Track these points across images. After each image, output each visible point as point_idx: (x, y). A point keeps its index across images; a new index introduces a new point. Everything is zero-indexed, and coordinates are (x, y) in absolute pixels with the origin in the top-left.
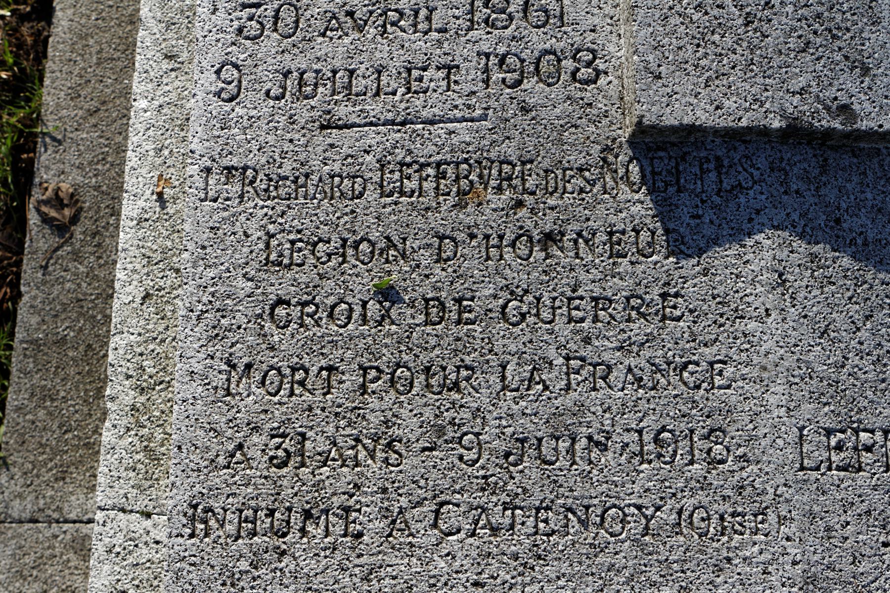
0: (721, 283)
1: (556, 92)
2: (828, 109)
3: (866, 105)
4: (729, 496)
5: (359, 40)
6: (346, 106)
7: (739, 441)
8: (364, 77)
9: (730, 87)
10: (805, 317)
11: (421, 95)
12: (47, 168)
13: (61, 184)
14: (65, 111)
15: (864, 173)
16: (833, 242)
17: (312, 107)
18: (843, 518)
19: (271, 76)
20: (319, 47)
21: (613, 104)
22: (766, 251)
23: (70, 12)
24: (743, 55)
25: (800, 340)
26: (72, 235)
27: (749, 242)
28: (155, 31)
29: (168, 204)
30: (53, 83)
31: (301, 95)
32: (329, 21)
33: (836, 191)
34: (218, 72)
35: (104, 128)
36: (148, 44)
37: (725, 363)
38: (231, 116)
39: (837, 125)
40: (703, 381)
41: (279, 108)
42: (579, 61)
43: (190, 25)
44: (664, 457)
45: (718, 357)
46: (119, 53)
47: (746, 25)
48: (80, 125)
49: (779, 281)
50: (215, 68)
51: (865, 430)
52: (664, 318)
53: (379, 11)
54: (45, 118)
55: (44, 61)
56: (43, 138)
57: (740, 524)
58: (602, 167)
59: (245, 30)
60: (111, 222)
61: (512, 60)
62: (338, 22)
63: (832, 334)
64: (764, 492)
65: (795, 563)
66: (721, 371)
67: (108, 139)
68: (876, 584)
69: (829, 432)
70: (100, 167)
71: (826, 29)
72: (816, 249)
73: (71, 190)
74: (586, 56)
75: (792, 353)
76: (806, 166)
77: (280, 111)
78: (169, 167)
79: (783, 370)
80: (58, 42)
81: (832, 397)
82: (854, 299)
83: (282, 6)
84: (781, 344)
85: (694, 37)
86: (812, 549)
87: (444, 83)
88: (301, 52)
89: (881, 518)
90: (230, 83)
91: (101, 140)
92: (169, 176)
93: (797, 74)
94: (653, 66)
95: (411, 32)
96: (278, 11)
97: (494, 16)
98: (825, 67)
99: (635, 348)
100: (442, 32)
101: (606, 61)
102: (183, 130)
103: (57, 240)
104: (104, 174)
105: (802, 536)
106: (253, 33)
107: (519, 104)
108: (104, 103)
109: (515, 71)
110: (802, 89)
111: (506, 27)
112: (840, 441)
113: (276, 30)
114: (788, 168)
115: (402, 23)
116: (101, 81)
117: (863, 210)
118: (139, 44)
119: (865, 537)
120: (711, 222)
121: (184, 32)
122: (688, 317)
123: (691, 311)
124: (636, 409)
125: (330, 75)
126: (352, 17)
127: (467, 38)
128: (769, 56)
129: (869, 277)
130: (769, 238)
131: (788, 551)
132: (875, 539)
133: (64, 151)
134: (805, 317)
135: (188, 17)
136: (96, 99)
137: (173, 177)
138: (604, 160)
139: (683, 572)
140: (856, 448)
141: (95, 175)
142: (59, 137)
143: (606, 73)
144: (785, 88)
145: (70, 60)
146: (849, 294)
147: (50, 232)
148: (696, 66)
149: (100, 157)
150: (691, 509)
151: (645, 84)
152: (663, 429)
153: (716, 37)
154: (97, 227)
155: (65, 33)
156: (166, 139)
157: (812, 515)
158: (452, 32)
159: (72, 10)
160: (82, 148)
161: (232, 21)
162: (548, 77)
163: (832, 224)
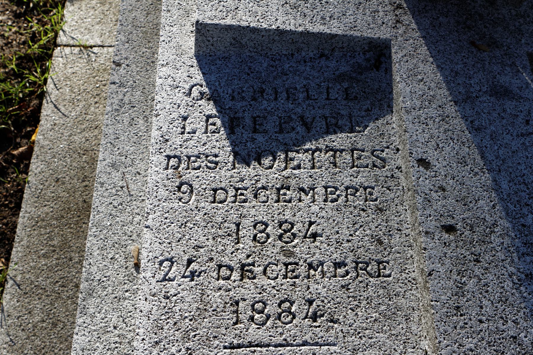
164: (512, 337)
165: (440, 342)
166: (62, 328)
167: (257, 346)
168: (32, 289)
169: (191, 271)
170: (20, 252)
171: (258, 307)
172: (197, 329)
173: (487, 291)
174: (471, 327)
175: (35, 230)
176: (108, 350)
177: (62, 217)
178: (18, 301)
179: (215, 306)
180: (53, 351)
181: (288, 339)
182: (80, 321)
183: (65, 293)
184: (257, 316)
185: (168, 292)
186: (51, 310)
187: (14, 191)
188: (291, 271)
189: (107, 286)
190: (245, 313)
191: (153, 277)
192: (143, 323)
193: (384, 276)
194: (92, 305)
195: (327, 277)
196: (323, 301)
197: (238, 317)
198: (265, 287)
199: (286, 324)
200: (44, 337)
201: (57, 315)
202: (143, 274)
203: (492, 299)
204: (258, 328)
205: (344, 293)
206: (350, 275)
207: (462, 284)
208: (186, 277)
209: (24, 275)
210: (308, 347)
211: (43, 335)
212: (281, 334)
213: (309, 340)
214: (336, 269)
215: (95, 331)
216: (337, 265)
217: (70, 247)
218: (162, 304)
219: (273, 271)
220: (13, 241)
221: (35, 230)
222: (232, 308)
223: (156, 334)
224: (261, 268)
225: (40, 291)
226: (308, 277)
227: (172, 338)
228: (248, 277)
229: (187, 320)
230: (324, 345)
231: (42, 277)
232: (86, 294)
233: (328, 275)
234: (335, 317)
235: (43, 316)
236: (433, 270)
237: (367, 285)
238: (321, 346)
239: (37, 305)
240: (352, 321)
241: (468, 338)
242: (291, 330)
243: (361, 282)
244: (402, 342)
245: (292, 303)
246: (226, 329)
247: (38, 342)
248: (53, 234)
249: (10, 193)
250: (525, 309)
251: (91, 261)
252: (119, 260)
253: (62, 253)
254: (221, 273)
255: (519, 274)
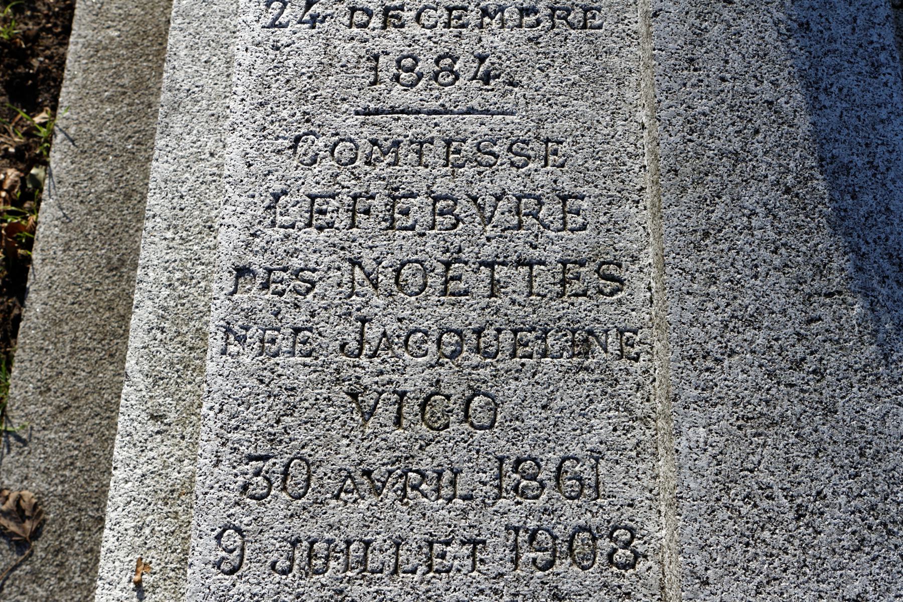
1: (592, 577)
5: (376, 505)
6: (361, 585)
8: (381, 550)
9: (782, 594)
11: (444, 574)
12: (9, 472)
13: (24, 492)
14: (33, 406)
17: (322, 585)
19: (278, 545)
20: (331, 512)
21: (653, 595)
23: (44, 294)
24: (795, 556)
26: (32, 551)
28: (142, 387)
29: (146, 594)
30: (21, 374)
31: (310, 571)
32: (344, 481)
34: (218, 538)
35: (74, 428)
36: (133, 402)
38: (231, 593)
41: (286, 585)
42: (616, 540)
43: (179, 381)
46: (95, 343)
47: (798, 519)
48: (48, 423)
50: (215, 533)
53: (399, 472)
54: (10, 414)
55: (12, 341)
56: (7, 437)
59: (251, 487)
60: (77, 538)
61: (544, 536)
62: (353, 482)
67: (78, 441)
70: (67, 473)
71: (881, 523)
73: (34, 501)
77: (286, 589)
78: (149, 549)
80: (30, 327)
83: (292, 460)
85: (743, 535)
87: (469, 562)
88: (312, 517)
90: (231, 551)
91: (70, 442)
92: (149, 559)
93: (852, 578)
94: (700, 570)
95: (433, 498)
96: (287, 466)
97: (524, 483)
98: (881, 568)
100: (470, 499)
101: (645, 543)
102: (166, 504)
103: (15, 557)
104: (72, 481)
106: (259, 491)
107: (550, 590)
108: (76, 399)
109: (546, 550)
111: (537, 497)
113: (284, 489)
115: (424, 487)
116: (74, 374)
118: (123, 402)
121: (173, 388)
125: (343, 546)
126: (369, 478)
127: (495, 508)
128: (822, 556)
133: (29, 453)
135: (177, 371)
136: (67, 395)
137: (154, 560)
141: (62, 482)
142: (25, 437)
143: (645, 557)
144: (840, 595)
145: (42, 349)
147: (7, 547)
148: (746, 569)
149: (69, 461)
151: (692, 592)
153: (766, 534)
154: (61, 543)
155: (37, 318)
156: (148, 515)
158: (479, 500)
159: (47, 292)
160: (48, 450)
161: (236, 475)
162: (583, 559)
164: (766, 101)
165: (659, 102)
166: (139, 202)
167: (402, 112)
168: (93, 146)
169: (311, 15)
170: (73, 93)
171: (407, 64)
172: (318, 89)
173: (738, 42)
174: (708, 86)
175: (93, 62)
176: (202, 183)
177: (135, 44)
178: (72, 163)
179: (344, 60)
180: (127, 232)
181: (447, 105)
182: (160, 143)
183: (143, 153)
184: (403, 75)
185: (278, 41)
186: (122, 177)
187: (61, 9)
188: (456, 17)
189: (200, 99)
190: (387, 71)
191: (257, 21)
192: (243, 80)
193: (591, 28)
194: (178, 123)
195: (509, 27)
196: (500, 58)
197: (376, 75)
198: (416, 38)
199: (446, 85)
200: (113, 212)
201: (131, 182)
202: (243, 17)
203: (744, 51)
204: (405, 90)
205: (531, 47)
206: (542, 25)
207: (702, 30)
208: (304, 23)
209: (80, 126)
210: (475, 116)
211: (112, 210)
212: (437, 98)
213: (477, 107)
214: (522, 17)
215: (182, 157)
216: (524, 11)
217: (148, 88)
218: (269, 57)
219: (429, 17)
220: (62, 79)
221: (93, 62)
222: (369, 64)
223: (260, 93)
224: (413, 13)
225: (106, 149)
226: (481, 26)
227: (283, 99)
228: (394, 24)
229: (304, 78)
230: (499, 114)
231: (107, 129)
232: (168, 109)
233: (510, 24)
234: (517, 78)
235: (110, 183)
236: (661, 10)
237: (566, 38)
238: (493, 115)
239: (101, 168)
240: (540, 84)
241: (702, 98)
242: (452, 94)
243: (558, 34)
244: (609, 112)
245: (455, 60)
246: (359, 90)
247: (104, 219)
248: (122, 68)
249: (54, 12)
250: (791, 68)
251: (175, 63)
252: (217, 64)
253: (136, 96)
254: (355, 18)
255: (789, 22)
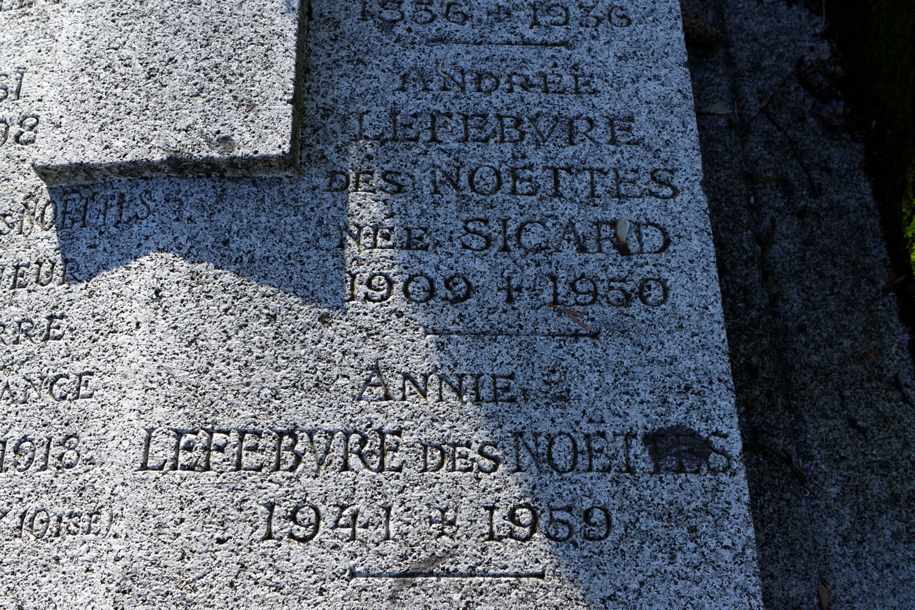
0: (102, 302)
2: (209, 142)
3: (247, 136)
4: (69, 498)
7: (89, 446)
10: (175, 328)
15: (263, 201)
16: (218, 260)
18: (178, 515)
22: (151, 269)
25: (165, 349)
27: (134, 264)
33: (230, 216)
37: (91, 374)
39: (215, 154)
40: (69, 392)
44: (19, 464)
45: (86, 369)
49: (154, 297)
51: (219, 431)
52: (47, 338)
57: (76, 525)
58: (23, 212)
63: (200, 343)
64: (102, 491)
65: (117, 559)
66: (87, 381)
68: (203, 580)
69: (179, 434)
72: (198, 267)
74: (30, 122)
75: (155, 361)
76: (203, 196)
79: (142, 376)
81: (188, 401)
82: (230, 311)
84: (144, 353)
86: (138, 545)
89: (220, 515)
99: (16, 367)
105: (129, 532)
110: (189, 126)
112: (189, 442)
114: (184, 198)
117: (255, 232)
119: (198, 534)
120: (105, 250)
122: (68, 335)
123: (71, 330)
124: (4, 422)
129: (250, 291)
130: (152, 260)
131: (113, 547)
132: (209, 535)
134: (175, 328)
138: (26, 205)
139: (13, 573)
140: (206, 449)
144: (173, 127)
146: (225, 306)
150: (33, 512)
152: (25, 439)
157: (145, 513)
163: (220, 245)
